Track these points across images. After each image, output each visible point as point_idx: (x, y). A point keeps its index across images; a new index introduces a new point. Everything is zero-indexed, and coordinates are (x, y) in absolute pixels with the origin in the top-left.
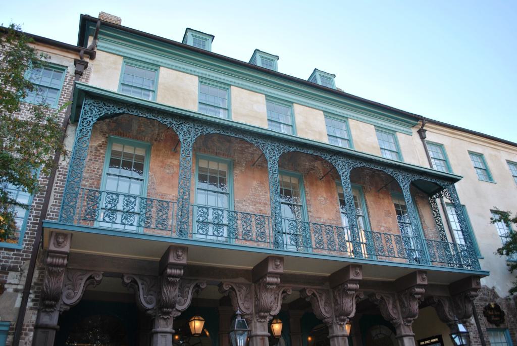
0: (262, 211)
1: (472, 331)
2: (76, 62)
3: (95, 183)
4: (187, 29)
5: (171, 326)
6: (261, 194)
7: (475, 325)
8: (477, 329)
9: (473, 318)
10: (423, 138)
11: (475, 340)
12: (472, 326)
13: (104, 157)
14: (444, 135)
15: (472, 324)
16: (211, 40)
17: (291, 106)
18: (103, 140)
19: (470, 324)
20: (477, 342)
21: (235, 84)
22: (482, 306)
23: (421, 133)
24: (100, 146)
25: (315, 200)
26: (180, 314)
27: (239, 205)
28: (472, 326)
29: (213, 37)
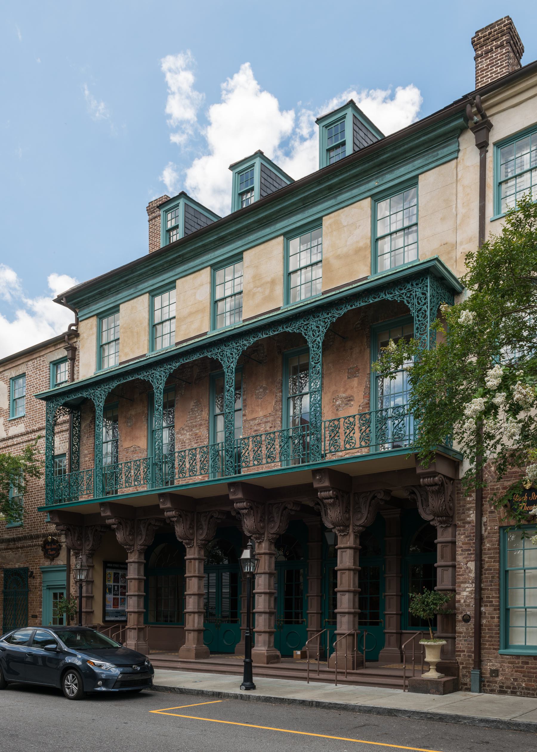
1: (464, 534)
12: (467, 526)
15: (469, 523)
20: (470, 550)
28: (467, 526)
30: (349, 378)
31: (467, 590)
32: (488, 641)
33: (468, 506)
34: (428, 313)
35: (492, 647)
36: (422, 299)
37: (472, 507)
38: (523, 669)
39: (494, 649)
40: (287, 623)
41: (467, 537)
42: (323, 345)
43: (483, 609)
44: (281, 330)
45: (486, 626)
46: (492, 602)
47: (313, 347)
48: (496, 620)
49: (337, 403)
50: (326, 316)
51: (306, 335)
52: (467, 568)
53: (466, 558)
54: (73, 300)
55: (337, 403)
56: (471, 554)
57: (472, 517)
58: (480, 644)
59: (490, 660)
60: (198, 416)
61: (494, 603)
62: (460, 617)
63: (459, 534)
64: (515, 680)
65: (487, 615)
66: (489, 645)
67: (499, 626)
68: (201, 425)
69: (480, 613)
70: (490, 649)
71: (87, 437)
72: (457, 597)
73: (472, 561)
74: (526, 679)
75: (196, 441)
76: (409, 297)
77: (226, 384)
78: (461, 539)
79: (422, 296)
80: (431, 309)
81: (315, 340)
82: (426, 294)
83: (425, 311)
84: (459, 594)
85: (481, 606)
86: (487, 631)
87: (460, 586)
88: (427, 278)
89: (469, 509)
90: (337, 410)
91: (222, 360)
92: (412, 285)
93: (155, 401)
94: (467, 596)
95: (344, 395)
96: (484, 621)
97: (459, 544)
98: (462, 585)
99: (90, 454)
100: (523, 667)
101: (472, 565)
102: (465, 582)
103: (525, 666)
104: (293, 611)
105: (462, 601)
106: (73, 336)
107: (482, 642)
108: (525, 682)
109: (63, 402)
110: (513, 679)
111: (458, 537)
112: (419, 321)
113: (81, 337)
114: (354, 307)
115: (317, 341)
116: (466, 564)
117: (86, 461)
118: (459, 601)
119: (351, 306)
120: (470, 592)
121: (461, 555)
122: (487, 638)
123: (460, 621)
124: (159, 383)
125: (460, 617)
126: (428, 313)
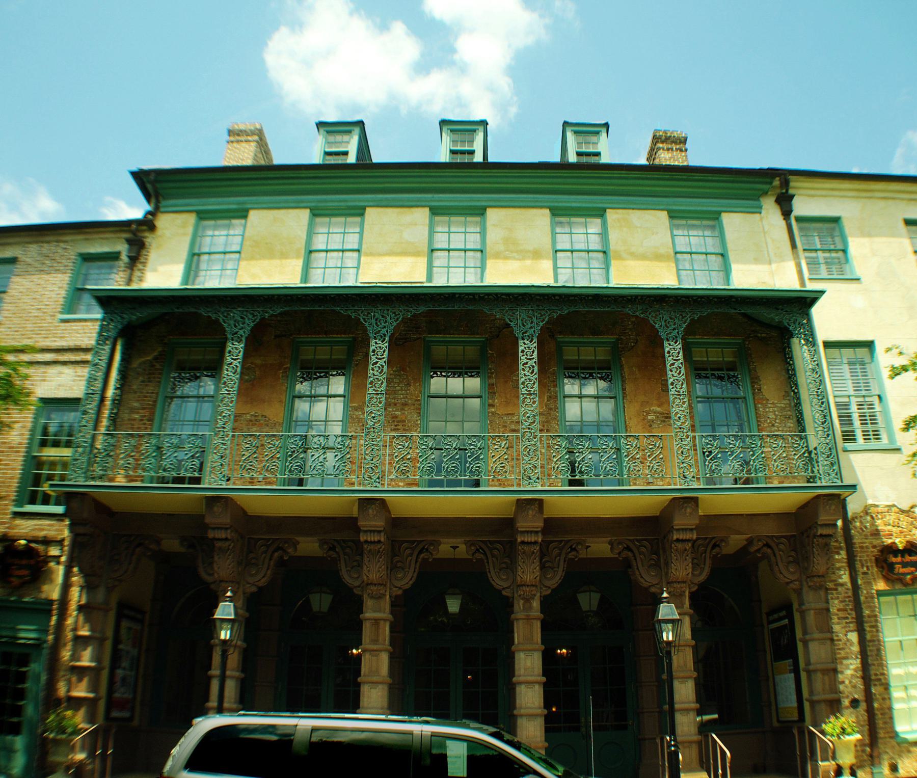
0: (396, 417)
1: (838, 598)
2: (129, 241)
3: (147, 414)
4: (260, 133)
5: (388, 608)
6: (398, 388)
7: (849, 585)
8: (850, 594)
9: (847, 573)
10: (786, 213)
11: (841, 614)
12: (840, 589)
13: (160, 374)
14: (842, 197)
15: (842, 585)
16: (604, 130)
17: (717, 219)
18: (160, 349)
19: (835, 585)
20: (847, 618)
21: (371, 204)
22: (874, 547)
23: (785, 203)
24: (156, 358)
25: (506, 382)
26: (549, 592)
27: (357, 413)
28: (840, 589)
29: (606, 125)
30: (555, 386)
31: (852, 667)
33: (838, 565)
37: (842, 567)
41: (842, 602)
45: (878, 709)
49: (649, 417)
52: (848, 640)
53: (844, 627)
54: (155, 184)
55: (649, 417)
56: (851, 622)
57: (845, 578)
60: (402, 390)
62: (846, 702)
63: (832, 598)
68: (405, 404)
71: (143, 382)
72: (841, 677)
73: (852, 631)
75: (393, 427)
78: (835, 605)
84: (842, 673)
87: (841, 663)
89: (839, 569)
90: (651, 426)
94: (852, 675)
95: (659, 409)
96: (876, 705)
97: (833, 610)
98: (845, 662)
99: (144, 409)
101: (853, 637)
102: (846, 658)
105: (847, 682)
106: (145, 228)
111: (831, 601)
113: (159, 232)
116: (846, 635)
117: (134, 420)
118: (843, 682)
120: (855, 670)
121: (838, 623)
123: (847, 708)
125: (846, 702)
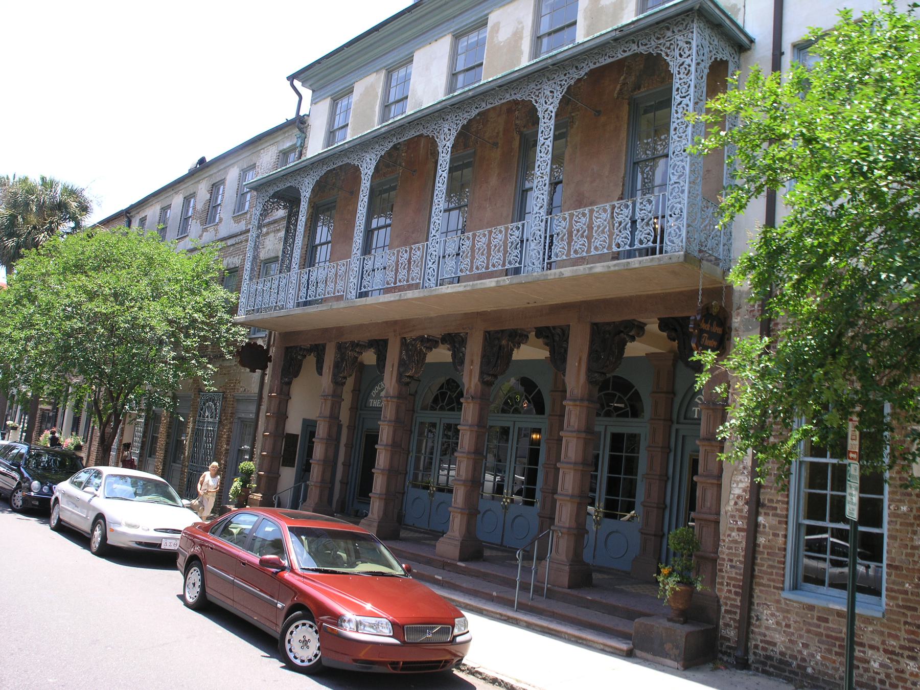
32: (765, 573)
34: (693, 69)
35: (772, 584)
36: (686, 50)
38: (819, 630)
39: (775, 587)
40: (607, 516)
42: (556, 116)
43: (761, 519)
44: (508, 97)
46: (776, 509)
47: (679, 73)
48: (781, 540)
50: (563, 78)
51: (667, 55)
58: (753, 576)
59: (768, 606)
61: (779, 511)
64: (805, 646)
65: (767, 529)
66: (769, 580)
67: (785, 549)
69: (757, 525)
70: (769, 586)
74: (823, 647)
76: (669, 48)
77: (540, 135)
79: (686, 46)
80: (698, 64)
81: (683, 63)
82: (690, 43)
83: (689, 66)
85: (757, 514)
86: (765, 556)
88: (693, 21)
91: (667, 55)
92: (673, 32)
93: (674, 89)
96: (762, 540)
100: (819, 626)
103: (823, 624)
104: (620, 498)
107: (756, 573)
108: (820, 652)
109: (272, 192)
110: (803, 644)
112: (680, 79)
114: (598, 65)
115: (686, 63)
119: (595, 64)
122: (764, 568)
124: (685, 56)
126: (693, 69)
